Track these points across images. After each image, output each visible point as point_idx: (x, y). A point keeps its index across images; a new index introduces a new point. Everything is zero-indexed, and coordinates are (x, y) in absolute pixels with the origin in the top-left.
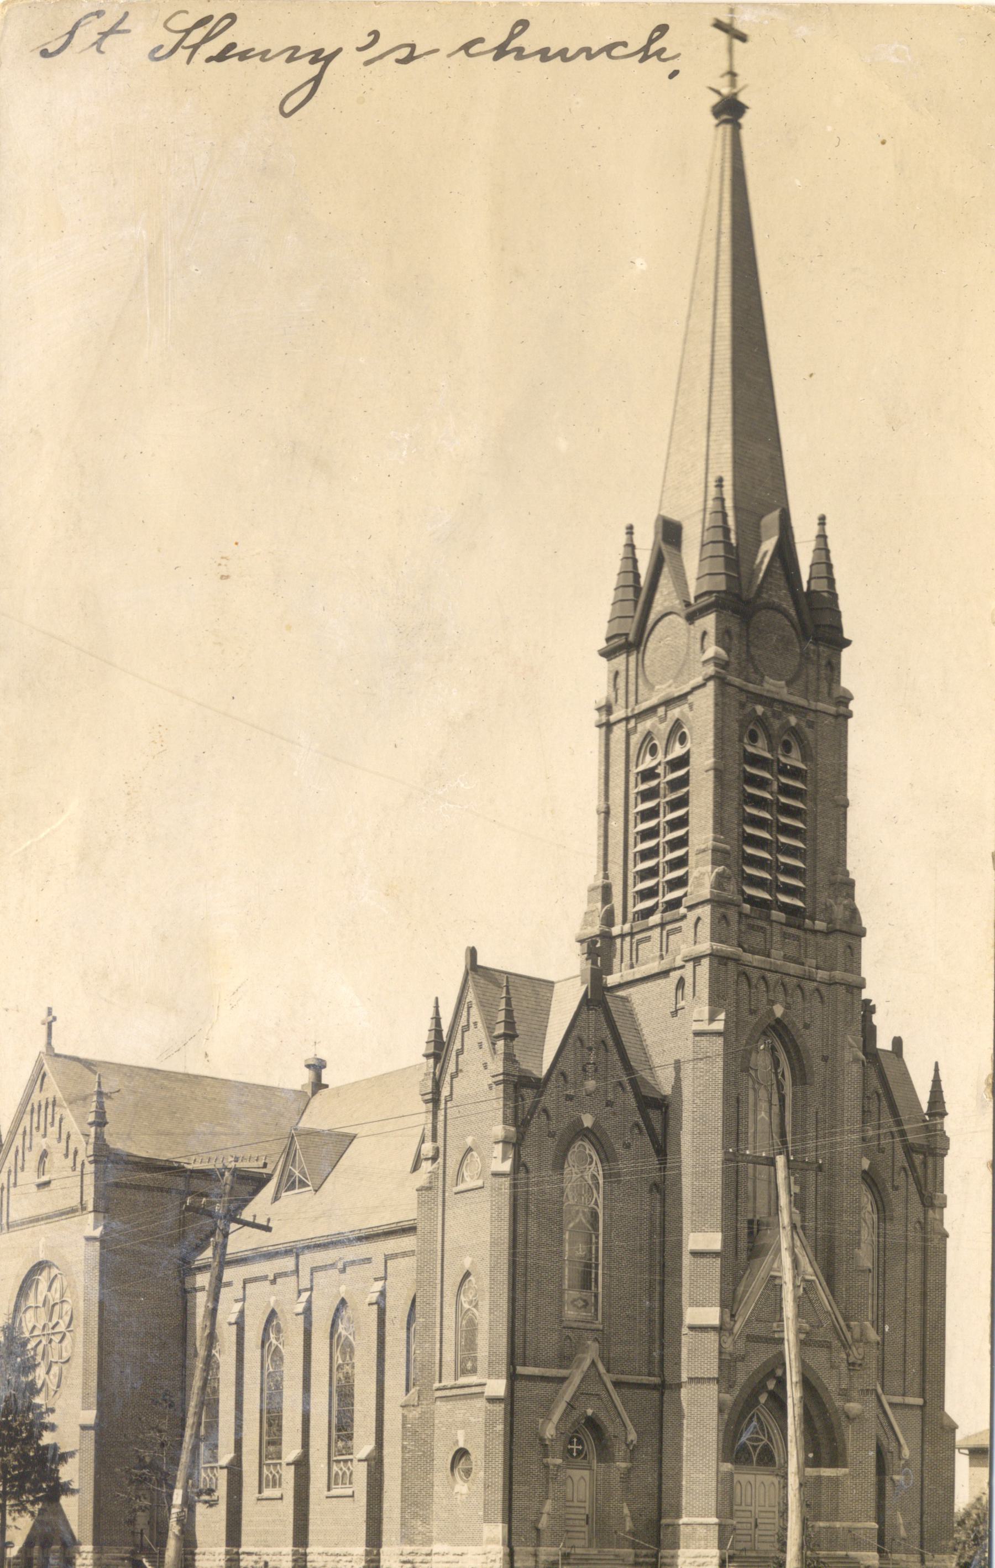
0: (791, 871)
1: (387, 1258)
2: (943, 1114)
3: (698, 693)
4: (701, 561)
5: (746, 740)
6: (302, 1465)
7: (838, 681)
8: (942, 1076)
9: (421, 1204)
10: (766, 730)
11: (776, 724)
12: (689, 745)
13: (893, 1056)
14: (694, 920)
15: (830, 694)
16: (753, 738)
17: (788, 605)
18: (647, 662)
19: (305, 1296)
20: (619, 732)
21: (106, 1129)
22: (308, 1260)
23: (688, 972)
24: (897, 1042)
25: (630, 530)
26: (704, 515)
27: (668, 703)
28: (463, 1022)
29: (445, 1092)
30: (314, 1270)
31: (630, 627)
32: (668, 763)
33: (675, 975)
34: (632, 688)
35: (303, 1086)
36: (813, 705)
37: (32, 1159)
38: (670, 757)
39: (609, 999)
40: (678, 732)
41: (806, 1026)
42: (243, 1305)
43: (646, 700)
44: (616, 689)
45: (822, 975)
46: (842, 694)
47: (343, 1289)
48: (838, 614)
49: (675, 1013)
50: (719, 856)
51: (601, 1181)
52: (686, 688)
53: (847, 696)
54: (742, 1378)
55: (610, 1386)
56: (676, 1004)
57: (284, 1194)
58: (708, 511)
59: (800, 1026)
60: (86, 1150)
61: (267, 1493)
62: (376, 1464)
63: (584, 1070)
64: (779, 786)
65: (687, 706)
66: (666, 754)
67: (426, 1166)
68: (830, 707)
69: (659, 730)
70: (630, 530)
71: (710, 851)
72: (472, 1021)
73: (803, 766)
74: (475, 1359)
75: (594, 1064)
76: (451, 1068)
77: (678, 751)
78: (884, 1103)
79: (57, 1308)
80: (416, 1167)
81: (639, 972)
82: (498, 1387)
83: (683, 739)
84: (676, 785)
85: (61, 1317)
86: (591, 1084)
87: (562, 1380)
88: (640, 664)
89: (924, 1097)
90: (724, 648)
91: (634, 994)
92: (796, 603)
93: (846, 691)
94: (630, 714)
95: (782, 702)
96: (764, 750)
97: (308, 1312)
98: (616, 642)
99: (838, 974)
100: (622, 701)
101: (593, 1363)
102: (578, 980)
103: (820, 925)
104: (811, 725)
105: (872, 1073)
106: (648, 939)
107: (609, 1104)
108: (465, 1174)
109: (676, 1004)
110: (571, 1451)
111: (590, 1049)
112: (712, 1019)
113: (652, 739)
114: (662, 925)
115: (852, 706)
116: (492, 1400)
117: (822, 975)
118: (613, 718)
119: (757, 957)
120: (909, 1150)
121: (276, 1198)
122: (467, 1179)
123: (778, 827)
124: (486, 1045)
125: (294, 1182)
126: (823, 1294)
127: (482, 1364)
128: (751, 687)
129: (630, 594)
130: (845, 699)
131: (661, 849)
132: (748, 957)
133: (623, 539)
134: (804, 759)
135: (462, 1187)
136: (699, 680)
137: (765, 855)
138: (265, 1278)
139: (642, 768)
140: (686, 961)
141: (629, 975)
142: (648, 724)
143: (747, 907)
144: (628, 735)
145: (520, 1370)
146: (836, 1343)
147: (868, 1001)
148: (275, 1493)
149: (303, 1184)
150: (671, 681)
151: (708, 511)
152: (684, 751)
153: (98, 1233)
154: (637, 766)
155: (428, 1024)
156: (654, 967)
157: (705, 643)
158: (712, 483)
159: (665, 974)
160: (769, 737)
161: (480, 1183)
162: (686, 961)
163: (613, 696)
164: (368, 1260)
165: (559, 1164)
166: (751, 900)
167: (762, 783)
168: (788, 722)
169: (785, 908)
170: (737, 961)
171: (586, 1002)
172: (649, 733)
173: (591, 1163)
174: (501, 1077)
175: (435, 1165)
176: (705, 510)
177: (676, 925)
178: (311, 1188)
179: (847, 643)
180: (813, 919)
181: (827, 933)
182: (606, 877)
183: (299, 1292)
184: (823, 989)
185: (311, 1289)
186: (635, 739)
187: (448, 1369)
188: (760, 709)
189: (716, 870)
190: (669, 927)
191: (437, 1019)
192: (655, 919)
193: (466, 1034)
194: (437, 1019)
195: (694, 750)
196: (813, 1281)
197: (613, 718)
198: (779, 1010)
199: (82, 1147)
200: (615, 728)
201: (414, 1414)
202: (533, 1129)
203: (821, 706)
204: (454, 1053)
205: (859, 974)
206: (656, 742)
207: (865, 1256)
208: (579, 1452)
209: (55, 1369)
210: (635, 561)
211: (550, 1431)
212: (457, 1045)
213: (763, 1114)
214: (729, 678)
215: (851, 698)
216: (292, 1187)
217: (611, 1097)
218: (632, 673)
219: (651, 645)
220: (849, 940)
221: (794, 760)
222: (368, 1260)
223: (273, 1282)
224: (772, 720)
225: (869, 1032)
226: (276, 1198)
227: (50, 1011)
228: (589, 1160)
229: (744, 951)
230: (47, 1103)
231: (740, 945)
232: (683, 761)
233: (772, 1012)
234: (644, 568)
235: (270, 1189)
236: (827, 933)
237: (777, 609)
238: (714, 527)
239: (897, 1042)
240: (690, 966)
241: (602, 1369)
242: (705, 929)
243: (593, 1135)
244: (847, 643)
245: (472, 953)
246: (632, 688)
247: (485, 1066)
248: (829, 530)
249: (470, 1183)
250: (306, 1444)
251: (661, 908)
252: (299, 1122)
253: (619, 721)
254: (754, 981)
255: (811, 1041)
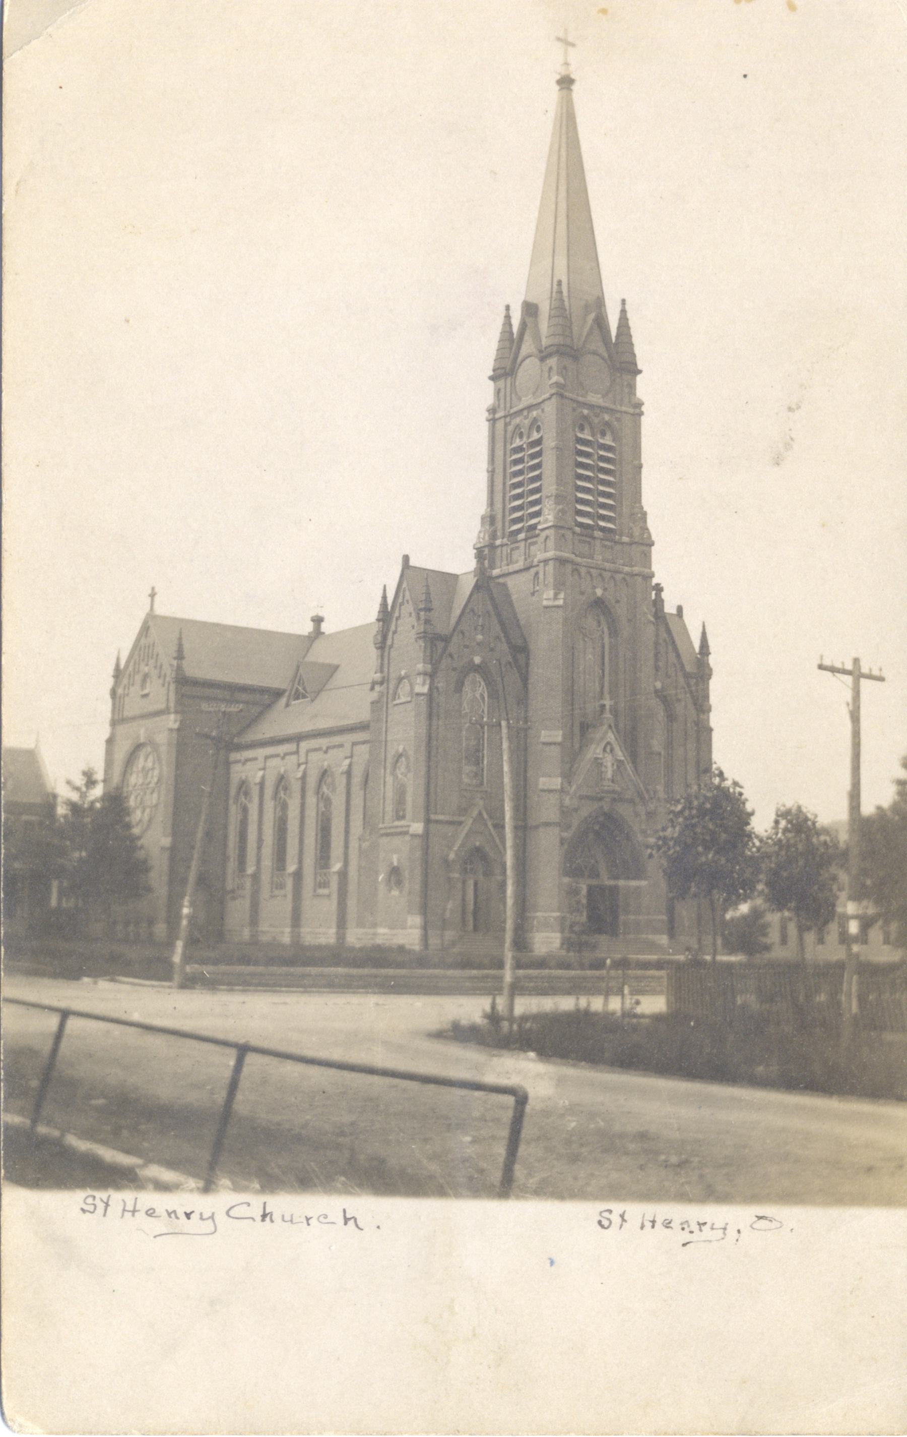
0: (603, 506)
1: (354, 744)
2: (708, 654)
3: (547, 403)
4: (548, 327)
5: (577, 430)
6: (298, 876)
7: (635, 395)
8: (707, 631)
9: (373, 711)
10: (590, 424)
11: (596, 420)
12: (542, 433)
13: (677, 618)
14: (544, 538)
15: (630, 402)
16: (582, 428)
17: (602, 350)
18: (517, 384)
19: (303, 767)
20: (500, 425)
21: (184, 662)
22: (304, 745)
23: (541, 569)
24: (680, 609)
25: (508, 308)
26: (551, 300)
27: (530, 408)
28: (400, 600)
29: (389, 642)
30: (308, 752)
31: (508, 364)
32: (529, 443)
33: (533, 571)
34: (508, 399)
35: (309, 633)
36: (619, 408)
37: (138, 678)
38: (530, 440)
39: (492, 585)
40: (536, 425)
41: (618, 602)
42: (264, 773)
43: (516, 406)
44: (499, 400)
45: (627, 569)
46: (637, 402)
47: (326, 764)
48: (634, 355)
49: (533, 594)
50: (559, 498)
51: (486, 699)
52: (540, 400)
53: (640, 402)
54: (575, 822)
55: (491, 827)
56: (534, 588)
57: (293, 702)
58: (553, 299)
59: (613, 601)
60: (170, 674)
61: (321, 891)
62: (343, 875)
63: (475, 629)
64: (598, 457)
65: (540, 410)
66: (529, 437)
67: (377, 688)
68: (630, 409)
69: (524, 424)
70: (508, 308)
71: (554, 497)
72: (405, 599)
73: (613, 444)
74: (404, 810)
75: (482, 625)
76: (393, 628)
77: (535, 436)
78: (670, 648)
79: (150, 772)
80: (372, 689)
81: (512, 568)
82: (418, 827)
83: (538, 429)
84: (533, 456)
85: (152, 777)
86: (480, 637)
87: (460, 823)
88: (513, 385)
89: (697, 645)
90: (563, 376)
91: (511, 582)
92: (608, 349)
93: (639, 399)
94: (507, 414)
95: (599, 407)
96: (588, 435)
97: (304, 778)
98: (499, 371)
99: (636, 569)
100: (502, 406)
101: (480, 814)
102: (472, 575)
103: (625, 539)
104: (618, 420)
105: (662, 630)
106: (518, 548)
107: (492, 650)
108: (401, 694)
109: (534, 588)
110: (465, 869)
111: (479, 616)
112: (556, 597)
113: (520, 428)
114: (526, 540)
115: (644, 409)
116: (414, 836)
117: (627, 569)
118: (497, 416)
119: (585, 560)
120: (687, 676)
121: (287, 705)
122: (402, 697)
123: (598, 481)
124: (413, 614)
125: (299, 695)
126: (629, 767)
127: (409, 814)
128: (580, 399)
129: (507, 344)
130: (639, 405)
131: (525, 494)
132: (579, 560)
133: (503, 313)
134: (614, 440)
135: (395, 702)
136: (547, 395)
137: (591, 498)
138: (277, 756)
139: (514, 445)
140: (539, 562)
141: (505, 569)
142: (517, 420)
143: (578, 529)
144: (506, 425)
145: (433, 817)
146: (637, 800)
147: (658, 585)
148: (325, 891)
149: (304, 697)
150: (531, 395)
151: (553, 299)
152: (539, 436)
153: (176, 726)
154: (511, 444)
155: (379, 600)
156: (520, 565)
157: (551, 374)
158: (555, 283)
159: (527, 569)
160: (592, 428)
161: (409, 699)
162: (539, 562)
163: (497, 403)
164: (341, 746)
165: (459, 687)
166: (581, 525)
167: (588, 455)
168: (603, 418)
169: (603, 529)
170: (572, 562)
171: (477, 587)
172: (518, 425)
173: (480, 686)
174: (422, 635)
175: (382, 688)
176: (551, 297)
177: (535, 540)
178: (309, 699)
179: (640, 372)
180: (621, 535)
181: (631, 544)
182: (492, 510)
183: (299, 765)
184: (628, 578)
185: (306, 763)
186: (510, 428)
187: (388, 817)
188: (586, 412)
189: (558, 508)
190: (529, 541)
191: (384, 597)
192: (522, 536)
193: (402, 607)
194: (384, 597)
195: (545, 437)
196: (623, 761)
197: (497, 416)
198: (599, 592)
199: (169, 672)
200: (497, 422)
201: (365, 845)
202: (443, 665)
203: (624, 409)
204: (394, 619)
205: (650, 568)
206: (522, 430)
207: (657, 744)
208: (472, 869)
209: (148, 811)
210: (510, 325)
211: (452, 856)
212: (396, 614)
213: (590, 656)
214: (566, 394)
215: (643, 404)
216: (297, 698)
217: (492, 645)
218: (508, 390)
219: (520, 373)
220: (644, 548)
221: (608, 441)
222: (341, 746)
223: (283, 758)
224: (593, 418)
225: (658, 603)
226: (287, 705)
227: (153, 589)
228: (479, 684)
229: (576, 556)
230: (145, 647)
231: (573, 553)
232: (539, 442)
233: (595, 593)
234: (515, 329)
235: (283, 701)
236: (631, 544)
237: (595, 353)
238: (556, 308)
239: (680, 609)
240: (542, 564)
241: (485, 816)
242: (551, 543)
243: (477, 669)
244: (640, 372)
245: (406, 558)
246: (508, 399)
247: (413, 627)
248: (627, 307)
249: (403, 700)
250: (300, 862)
251: (525, 529)
252: (306, 655)
253: (500, 418)
254: (583, 574)
255: (621, 611)
